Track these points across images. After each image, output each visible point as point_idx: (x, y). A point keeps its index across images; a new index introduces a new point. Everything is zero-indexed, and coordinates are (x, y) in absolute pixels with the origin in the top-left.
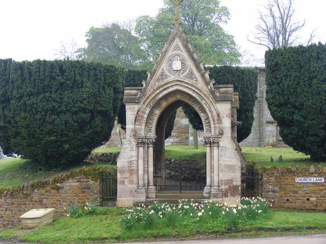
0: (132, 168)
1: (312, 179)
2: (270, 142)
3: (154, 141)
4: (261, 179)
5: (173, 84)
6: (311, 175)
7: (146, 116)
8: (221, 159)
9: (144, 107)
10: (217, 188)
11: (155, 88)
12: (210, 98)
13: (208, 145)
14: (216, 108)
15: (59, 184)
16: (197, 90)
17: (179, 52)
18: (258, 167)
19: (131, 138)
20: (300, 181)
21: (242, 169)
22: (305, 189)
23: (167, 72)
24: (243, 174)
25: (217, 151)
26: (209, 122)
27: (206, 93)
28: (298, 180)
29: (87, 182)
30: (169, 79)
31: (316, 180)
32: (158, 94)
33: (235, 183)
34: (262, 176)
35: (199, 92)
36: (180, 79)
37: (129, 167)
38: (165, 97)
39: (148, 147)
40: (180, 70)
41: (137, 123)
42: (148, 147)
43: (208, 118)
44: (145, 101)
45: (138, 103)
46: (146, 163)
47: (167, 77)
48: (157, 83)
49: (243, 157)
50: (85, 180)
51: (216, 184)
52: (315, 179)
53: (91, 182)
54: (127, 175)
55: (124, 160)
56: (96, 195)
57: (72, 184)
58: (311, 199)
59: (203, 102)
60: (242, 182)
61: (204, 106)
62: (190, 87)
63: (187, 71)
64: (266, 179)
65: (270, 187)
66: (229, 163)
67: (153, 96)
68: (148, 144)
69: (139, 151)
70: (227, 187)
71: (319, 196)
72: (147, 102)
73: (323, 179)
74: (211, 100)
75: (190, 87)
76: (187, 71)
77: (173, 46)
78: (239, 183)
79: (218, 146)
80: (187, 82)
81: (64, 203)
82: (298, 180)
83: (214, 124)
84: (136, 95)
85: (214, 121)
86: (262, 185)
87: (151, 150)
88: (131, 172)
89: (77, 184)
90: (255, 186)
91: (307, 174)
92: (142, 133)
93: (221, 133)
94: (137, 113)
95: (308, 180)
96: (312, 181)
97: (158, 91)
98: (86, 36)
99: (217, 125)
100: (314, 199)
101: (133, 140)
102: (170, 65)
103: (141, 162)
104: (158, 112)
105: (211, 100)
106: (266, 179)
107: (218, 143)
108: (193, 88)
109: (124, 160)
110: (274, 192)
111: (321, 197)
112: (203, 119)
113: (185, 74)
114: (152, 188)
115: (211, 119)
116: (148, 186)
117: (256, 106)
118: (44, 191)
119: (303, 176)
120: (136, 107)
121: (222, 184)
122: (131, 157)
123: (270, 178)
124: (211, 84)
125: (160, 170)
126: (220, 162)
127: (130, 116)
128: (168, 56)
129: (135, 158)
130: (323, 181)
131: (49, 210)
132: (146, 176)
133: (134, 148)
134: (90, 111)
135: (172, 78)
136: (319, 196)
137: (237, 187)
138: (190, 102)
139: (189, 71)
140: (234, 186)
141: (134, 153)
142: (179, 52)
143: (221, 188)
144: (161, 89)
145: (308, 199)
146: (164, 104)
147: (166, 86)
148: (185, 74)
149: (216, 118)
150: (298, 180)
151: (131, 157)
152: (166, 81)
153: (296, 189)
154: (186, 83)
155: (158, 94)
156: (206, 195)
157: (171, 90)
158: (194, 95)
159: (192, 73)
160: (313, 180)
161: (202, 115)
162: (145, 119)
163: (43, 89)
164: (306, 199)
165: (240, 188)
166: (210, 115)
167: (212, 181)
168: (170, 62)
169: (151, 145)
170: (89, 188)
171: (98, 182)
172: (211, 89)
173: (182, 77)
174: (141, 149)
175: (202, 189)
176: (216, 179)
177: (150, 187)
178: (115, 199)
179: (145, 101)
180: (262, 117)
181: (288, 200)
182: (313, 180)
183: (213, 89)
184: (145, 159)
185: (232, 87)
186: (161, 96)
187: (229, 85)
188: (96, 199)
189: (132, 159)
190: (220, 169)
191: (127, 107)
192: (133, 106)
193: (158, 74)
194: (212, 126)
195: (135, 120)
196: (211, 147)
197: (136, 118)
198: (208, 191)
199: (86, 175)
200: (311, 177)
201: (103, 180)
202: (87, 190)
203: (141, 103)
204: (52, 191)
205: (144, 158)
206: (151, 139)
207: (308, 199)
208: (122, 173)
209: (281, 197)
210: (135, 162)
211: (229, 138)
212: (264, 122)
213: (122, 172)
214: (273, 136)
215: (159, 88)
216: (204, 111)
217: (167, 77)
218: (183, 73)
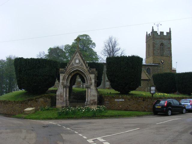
6: (120, 98)
26: (87, 81)
32: (71, 71)
43: (87, 79)
46: (66, 93)
47: (74, 65)
49: (98, 92)
51: (89, 101)
53: (48, 99)
59: (85, 74)
60: (98, 100)
78: (97, 101)
82: (116, 100)
87: (68, 89)
93: (91, 84)
102: (75, 61)
103: (64, 93)
104: (70, 77)
112: (85, 79)
120: (63, 75)
135: (75, 65)
141: (62, 90)
146: (73, 74)
155: (71, 71)
157: (75, 69)
158: (83, 71)
159: (82, 64)
160: (121, 100)
161: (85, 78)
167: (88, 100)
174: (65, 89)
175: (84, 102)
176: (89, 99)
182: (121, 100)
194: (88, 82)
216: (86, 77)
217: (74, 65)
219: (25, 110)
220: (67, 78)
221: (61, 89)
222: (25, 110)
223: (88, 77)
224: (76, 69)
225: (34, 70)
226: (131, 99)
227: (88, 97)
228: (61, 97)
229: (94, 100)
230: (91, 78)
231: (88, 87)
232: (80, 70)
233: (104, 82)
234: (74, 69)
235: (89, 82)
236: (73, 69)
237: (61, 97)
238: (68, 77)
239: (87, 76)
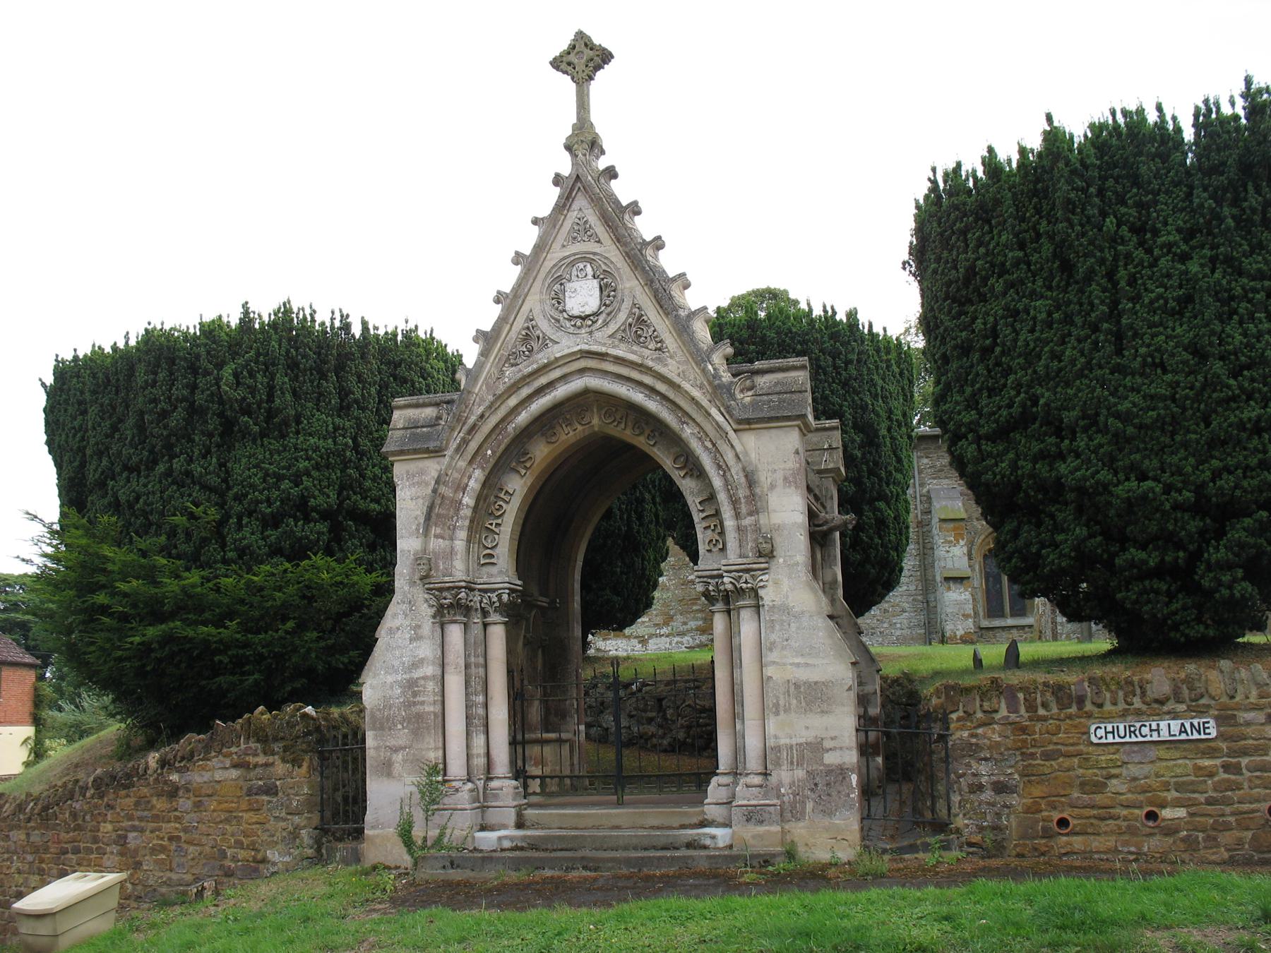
0: (419, 708)
1: (1163, 724)
2: (959, 634)
3: (505, 597)
4: (943, 738)
5: (566, 370)
6: (1157, 707)
7: (468, 500)
8: (771, 657)
9: (462, 464)
10: (757, 780)
11: (501, 388)
12: (714, 412)
13: (719, 606)
14: (739, 448)
15: (174, 777)
16: (661, 387)
17: (591, 247)
18: (932, 699)
19: (414, 590)
20: (1110, 739)
21: (863, 700)
22: (1134, 770)
23: (544, 326)
24: (865, 722)
25: (755, 624)
26: (717, 514)
27: (696, 393)
28: (1101, 733)
29: (266, 765)
30: (557, 351)
31: (1183, 730)
32: (515, 411)
33: (831, 759)
34: (945, 722)
35: (671, 394)
36: (595, 348)
37: (409, 705)
38: (545, 423)
39: (485, 625)
40: (596, 314)
41: (434, 530)
42: (485, 625)
43: (711, 498)
44: (465, 442)
45: (437, 452)
46: (477, 684)
47: (545, 341)
48: (509, 372)
49: (865, 661)
50: (261, 759)
51: (753, 763)
52: (1175, 725)
53: (280, 768)
54: (401, 736)
55: (390, 679)
56: (297, 819)
57: (218, 775)
58: (1167, 813)
59: (688, 432)
60: (865, 750)
61: (695, 445)
62: (635, 375)
63: (622, 316)
64: (966, 734)
65: (983, 769)
66: (803, 675)
67: (493, 420)
68: (485, 613)
69: (447, 639)
70: (800, 773)
71: (1202, 798)
72: (473, 446)
73: (1212, 723)
74: (720, 418)
75: (635, 375)
76: (622, 316)
77: (568, 224)
78: (851, 757)
79: (758, 608)
80: (620, 353)
81: (191, 849)
82: (1099, 733)
83: (737, 516)
84: (433, 423)
85: (735, 502)
86: (946, 760)
87: (498, 634)
88: (417, 723)
89: (234, 773)
90: (920, 765)
91: (1137, 702)
92: (459, 570)
93: (767, 554)
94: (435, 491)
95: (1145, 730)
96: (1165, 736)
97: (513, 402)
98: (365, 324)
99: (748, 521)
100: (1181, 813)
101: (420, 595)
102: (559, 300)
103: (455, 683)
104: (518, 487)
105: (720, 418)
106: (966, 734)
107: (755, 592)
108: (648, 380)
109: (390, 679)
110: (1000, 788)
111: (1210, 802)
112: (693, 502)
113: (612, 327)
114: (505, 786)
115: (722, 497)
116: (489, 779)
117: (912, 548)
118: (130, 801)
119: (1123, 715)
120: (432, 467)
121: (778, 764)
122: (416, 665)
123: (980, 731)
124: (718, 359)
125: (563, 715)
126: (769, 671)
127: (411, 504)
128: (548, 264)
129: (430, 670)
130: (1213, 733)
131: (111, 878)
132: (479, 741)
133: (427, 626)
134: (326, 515)
135: (566, 345)
136: (1202, 798)
137: (842, 771)
138: (642, 439)
139: (631, 314)
140: (830, 771)
141: (427, 650)
142: (591, 247)
143: (773, 779)
144: (525, 392)
145: (1151, 816)
146: (541, 452)
147: (543, 380)
148: (612, 327)
149: (742, 493)
150: (1101, 733)
151: (416, 665)
152: (542, 358)
153: (1098, 775)
154: (619, 360)
155: (515, 411)
156: (712, 811)
157: (561, 391)
158: (652, 405)
159: (641, 321)
160: (1169, 728)
161: (688, 486)
162: (467, 512)
163: (169, 447)
164: (1141, 813)
165: (854, 778)
166: (717, 483)
167: (738, 752)
168: (557, 287)
169: (495, 617)
170: (271, 790)
171: (305, 765)
172: (716, 376)
173: (600, 341)
174: (455, 633)
175: (701, 780)
176: (753, 743)
177: (494, 784)
178: (358, 833)
179: (465, 442)
180: (933, 567)
181: (1063, 823)
182: (1169, 728)
183: (726, 377)
184: (473, 670)
185: (803, 367)
186: (523, 418)
187: (793, 361)
188: (294, 835)
189: (417, 674)
190: (770, 702)
191: (400, 470)
192: (421, 464)
193: (513, 334)
194: (729, 523)
195: (428, 517)
196: (729, 612)
197: (431, 508)
198: (722, 795)
199: (264, 738)
200: (1160, 716)
201: (323, 757)
202: (265, 798)
203: (449, 453)
204: (154, 800)
205: (467, 666)
206: (493, 591)
207: (1151, 816)
208: (382, 728)
209: (1033, 809)
210: (431, 686)
211: (803, 573)
212: (938, 578)
213: (384, 725)
214: (966, 616)
215: (514, 387)
216: (695, 469)
217: (545, 341)
218: (606, 324)
219: (21, 905)
220: (480, 498)
221: (416, 638)
222: (21, 905)
223: (723, 468)
224: (576, 385)
225: (177, 464)
226: (697, 914)
227: (736, 715)
228: (417, 734)
229: (817, 747)
230: (764, 478)
231: (727, 598)
232: (622, 390)
233: (927, 586)
234: (551, 385)
235: (739, 529)
236: (540, 391)
237: (417, 734)
238: (491, 487)
239: (707, 461)
